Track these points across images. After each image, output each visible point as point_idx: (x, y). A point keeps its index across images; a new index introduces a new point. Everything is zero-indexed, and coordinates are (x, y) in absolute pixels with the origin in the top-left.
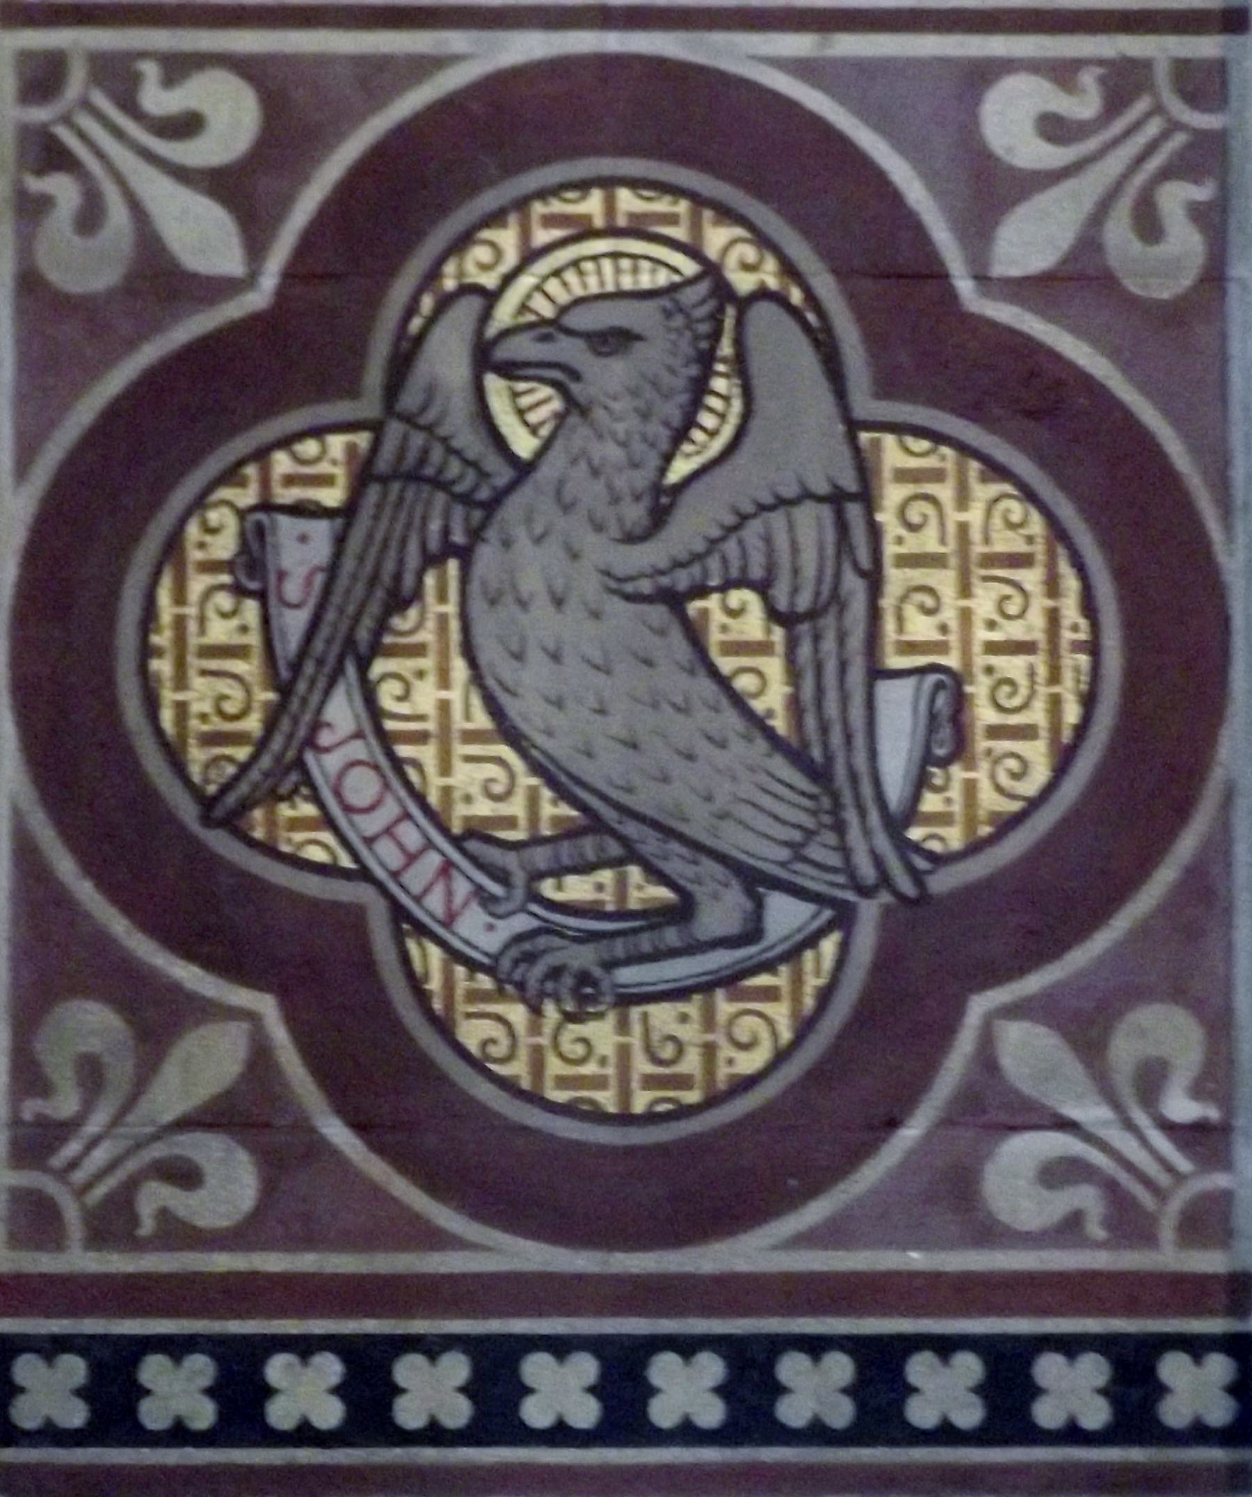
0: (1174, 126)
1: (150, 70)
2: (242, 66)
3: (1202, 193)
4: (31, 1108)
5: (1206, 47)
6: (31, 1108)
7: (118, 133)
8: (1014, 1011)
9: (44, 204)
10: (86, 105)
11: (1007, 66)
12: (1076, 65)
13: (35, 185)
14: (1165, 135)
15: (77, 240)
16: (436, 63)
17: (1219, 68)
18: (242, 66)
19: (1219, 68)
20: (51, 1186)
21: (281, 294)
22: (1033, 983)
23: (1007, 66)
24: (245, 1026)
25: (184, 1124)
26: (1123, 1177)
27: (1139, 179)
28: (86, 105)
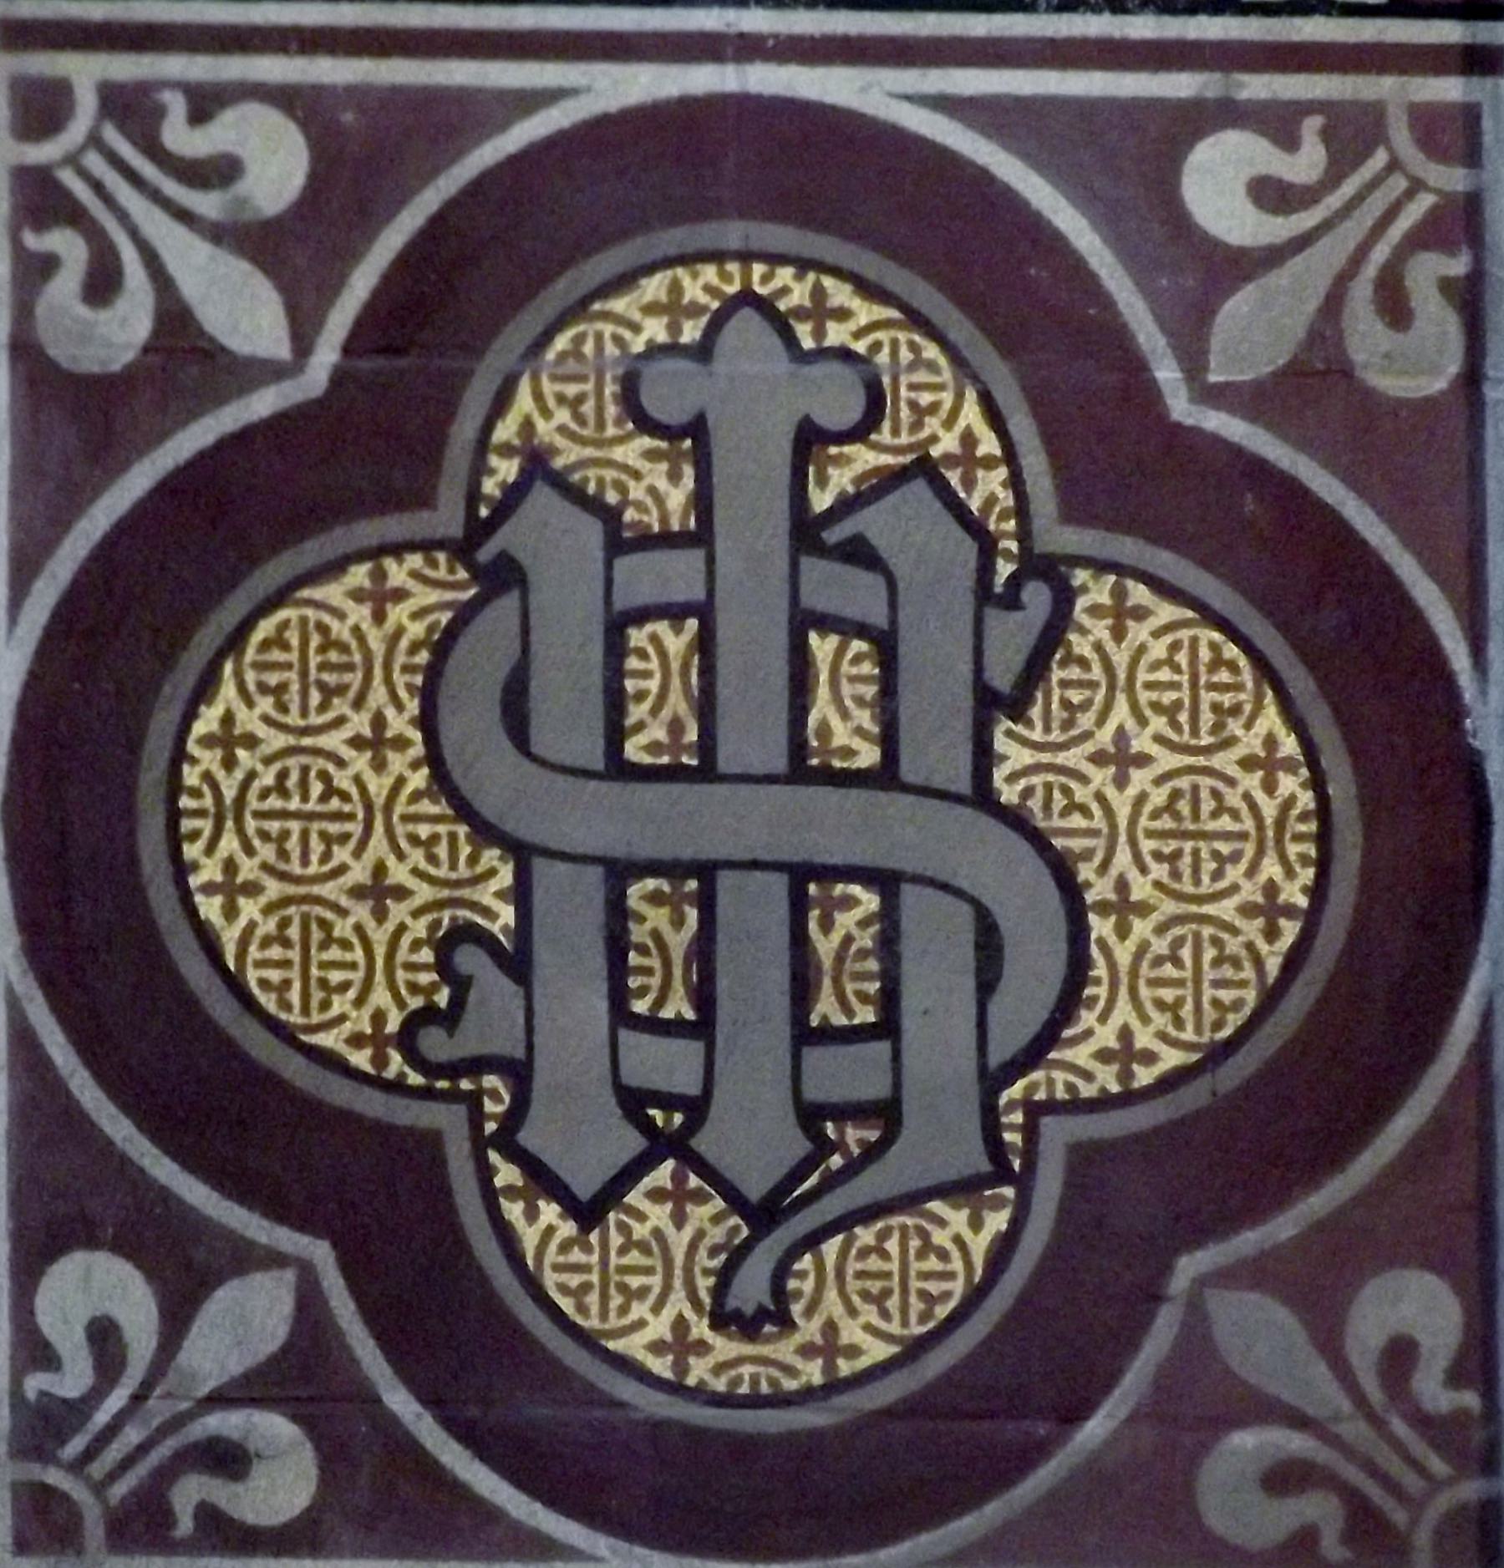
0: (95, 140)
1: (176, 105)
2: (284, 98)
3: (1458, 266)
4: (35, 1383)
5: (1449, 89)
6: (35, 1383)
8: (1225, 1277)
9: (48, 265)
10: (1417, 186)
12: (1295, 112)
14: (1410, 194)
15: (83, 311)
17: (1470, 115)
18: (284, 98)
19: (1470, 115)
20: (54, 1477)
21: (339, 378)
22: (1248, 1241)
24: (1208, 1292)
25: (219, 1400)
26: (1374, 1492)
27: (1380, 253)
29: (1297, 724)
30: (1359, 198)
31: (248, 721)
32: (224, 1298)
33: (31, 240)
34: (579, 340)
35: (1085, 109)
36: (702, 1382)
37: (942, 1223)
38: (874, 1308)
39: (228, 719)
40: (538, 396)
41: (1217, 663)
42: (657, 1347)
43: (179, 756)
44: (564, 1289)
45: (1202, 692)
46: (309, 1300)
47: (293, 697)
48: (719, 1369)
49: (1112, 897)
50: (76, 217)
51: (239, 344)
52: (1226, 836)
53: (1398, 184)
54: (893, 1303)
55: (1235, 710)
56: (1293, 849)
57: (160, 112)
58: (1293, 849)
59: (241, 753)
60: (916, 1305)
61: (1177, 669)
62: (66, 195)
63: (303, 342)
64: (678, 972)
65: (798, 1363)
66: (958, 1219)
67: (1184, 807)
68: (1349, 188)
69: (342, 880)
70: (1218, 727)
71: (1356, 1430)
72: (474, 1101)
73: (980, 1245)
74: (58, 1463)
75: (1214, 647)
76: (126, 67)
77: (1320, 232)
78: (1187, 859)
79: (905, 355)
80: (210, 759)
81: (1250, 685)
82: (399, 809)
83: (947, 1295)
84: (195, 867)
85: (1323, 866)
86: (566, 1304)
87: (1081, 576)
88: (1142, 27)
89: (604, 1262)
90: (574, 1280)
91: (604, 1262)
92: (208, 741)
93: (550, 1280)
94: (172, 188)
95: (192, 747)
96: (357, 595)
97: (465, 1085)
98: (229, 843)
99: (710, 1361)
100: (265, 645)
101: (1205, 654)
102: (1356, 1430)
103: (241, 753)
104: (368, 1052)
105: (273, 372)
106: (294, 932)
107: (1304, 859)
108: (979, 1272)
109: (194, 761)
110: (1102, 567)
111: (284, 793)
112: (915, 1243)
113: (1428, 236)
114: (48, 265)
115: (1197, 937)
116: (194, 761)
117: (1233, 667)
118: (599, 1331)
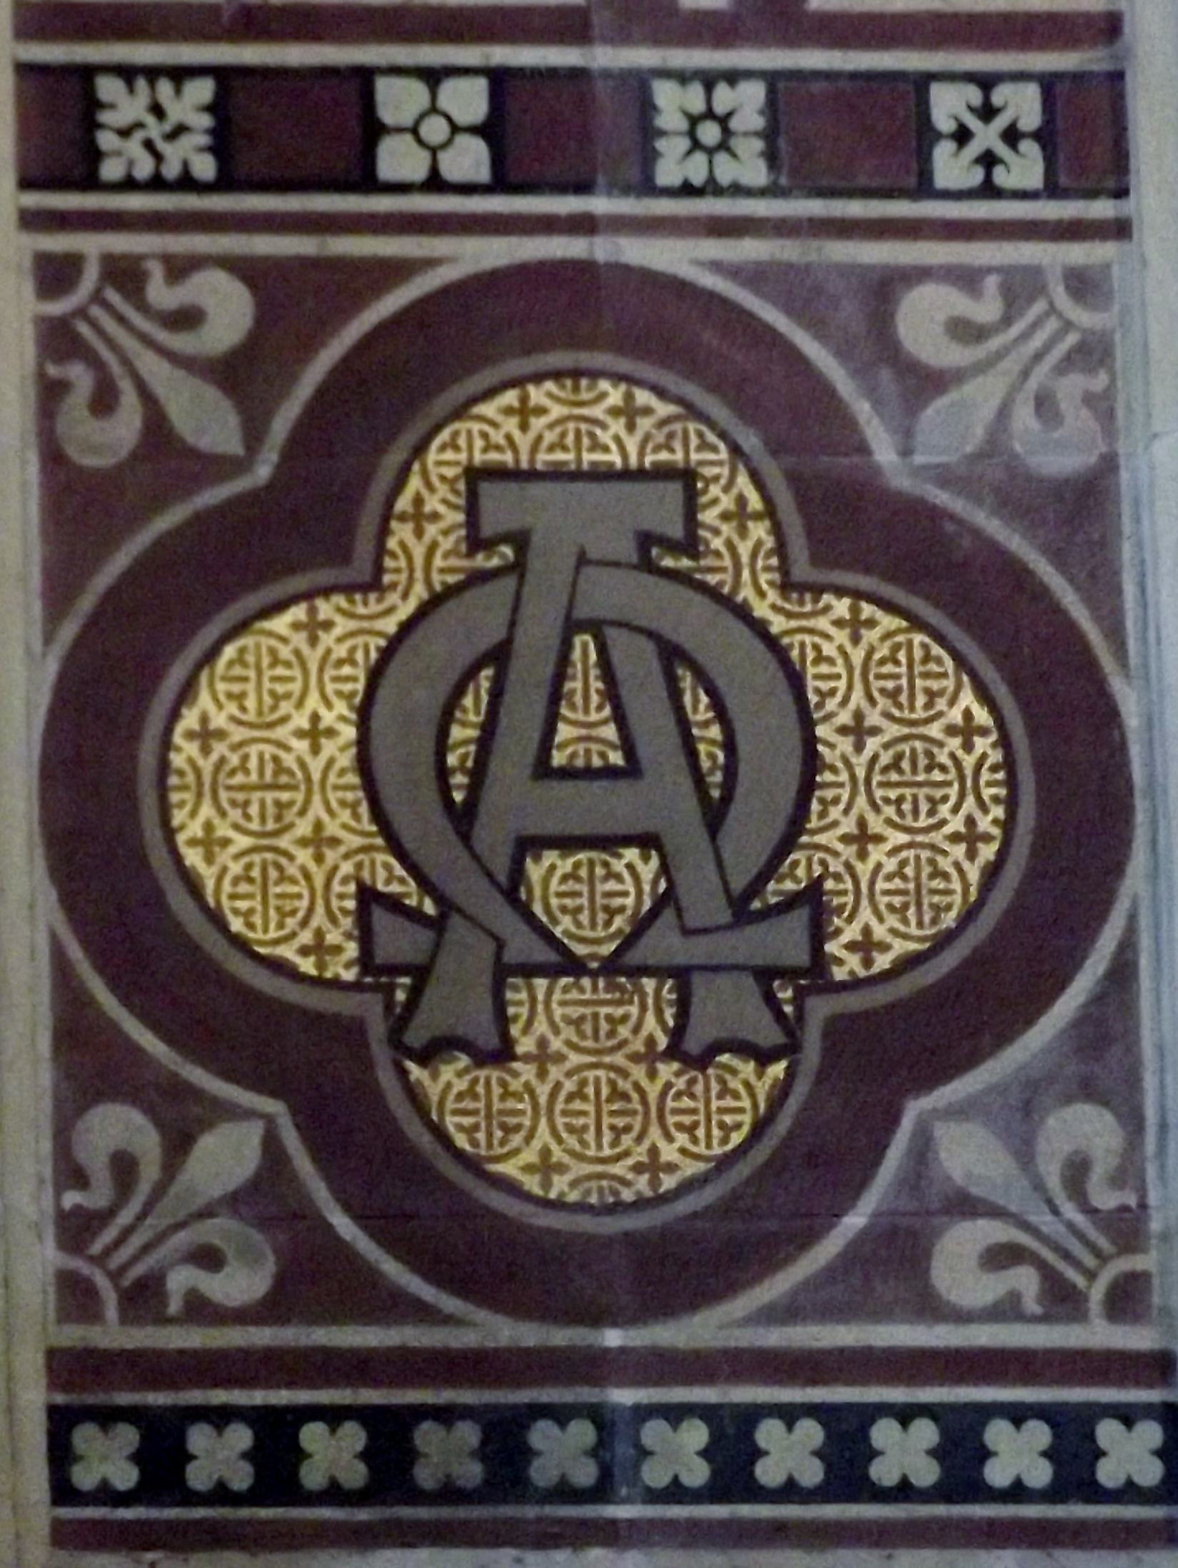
1: (156, 271)
2: (233, 265)
8: (237, 466)
11: (922, 274)
16: (399, 270)
18: (233, 265)
23: (922, 274)
31: (219, 721)
32: (207, 1143)
34: (456, 434)
36: (615, 386)
37: (734, 1072)
38: (686, 1136)
40: (752, 1095)
41: (927, 658)
45: (917, 681)
46: (271, 1144)
51: (205, 443)
54: (701, 1133)
58: (987, 793)
64: (537, 892)
65: (546, 402)
66: (748, 1068)
67: (905, 765)
69: (886, 739)
72: (390, 989)
73: (763, 1089)
75: (924, 646)
76: (121, 243)
81: (951, 671)
84: (994, 745)
85: (1011, 803)
87: (349, 975)
88: (855, 208)
89: (489, 1106)
90: (467, 1121)
91: (489, 1106)
95: (178, 738)
96: (885, 948)
97: (383, 979)
98: (206, 810)
99: (568, 1177)
101: (918, 654)
104: (312, 959)
107: (996, 799)
108: (762, 1106)
109: (179, 749)
110: (336, 984)
111: (930, 799)
114: (1118, 1180)
115: (918, 858)
117: (939, 661)
118: (484, 1157)
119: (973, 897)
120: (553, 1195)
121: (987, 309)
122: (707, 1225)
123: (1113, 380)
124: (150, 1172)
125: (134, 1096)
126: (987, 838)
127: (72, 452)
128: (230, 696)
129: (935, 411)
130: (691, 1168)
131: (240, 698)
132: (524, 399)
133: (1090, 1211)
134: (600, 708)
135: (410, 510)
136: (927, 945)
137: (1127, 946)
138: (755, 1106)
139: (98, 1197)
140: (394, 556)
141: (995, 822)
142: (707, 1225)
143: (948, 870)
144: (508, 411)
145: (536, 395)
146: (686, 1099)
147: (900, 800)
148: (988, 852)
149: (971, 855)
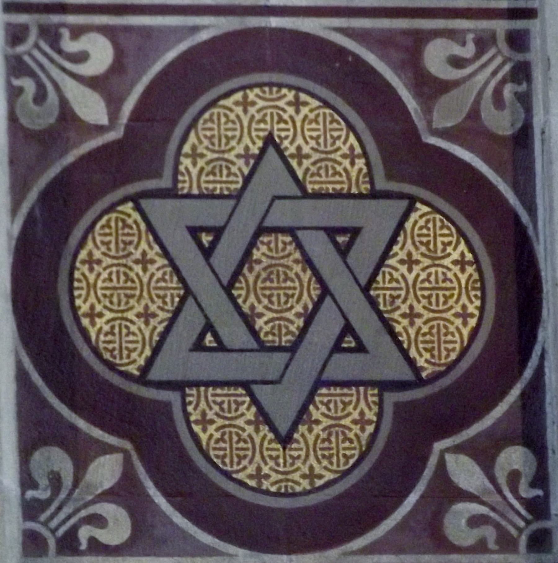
2: (105, 30)
4: (30, 494)
7: (52, 60)
13: (17, 82)
16: (195, 29)
18: (105, 30)
28: (37, 46)
29: (471, 249)
30: (69, 517)
33: (540, 492)
35: (392, 32)
39: (90, 254)
42: (251, 477)
43: (73, 268)
44: (217, 457)
47: (113, 246)
48: (273, 484)
49: (408, 311)
50: (32, 74)
52: (290, 288)
53: (54, 524)
55: (450, 243)
56: (472, 293)
57: (497, 542)
59: (95, 266)
60: (342, 460)
61: (429, 229)
62: (28, 66)
63: (114, 115)
68: (73, 521)
70: (444, 250)
71: (55, 72)
74: (39, 522)
77: (68, 518)
78: (434, 297)
79: (227, 460)
80: (471, 309)
82: (456, 292)
83: (353, 455)
85: (483, 299)
86: (218, 461)
92: (83, 262)
93: (212, 453)
94: (68, 65)
95: (477, 313)
100: (103, 227)
102: (55, 72)
103: (95, 266)
105: (100, 129)
106: (117, 330)
112: (341, 437)
113: (44, 505)
115: (439, 325)
116: (78, 269)
119: (465, 343)
120: (375, 419)
121: (469, 51)
122: (511, 276)
123: (23, 494)
124: (68, 480)
125: (63, 444)
126: (472, 315)
127: (24, 121)
128: (103, 243)
129: (445, 99)
130: (329, 476)
131: (107, 244)
132: (245, 97)
133: (519, 498)
134: (207, 189)
135: (190, 152)
136: (339, 475)
137: (540, 372)
138: (361, 446)
139: (42, 494)
140: (183, 174)
141: (476, 308)
142: (511, 276)
143: (444, 351)
144: (237, 103)
145: (251, 95)
146: (343, 437)
147: (429, 297)
148: (473, 322)
149: (465, 324)
